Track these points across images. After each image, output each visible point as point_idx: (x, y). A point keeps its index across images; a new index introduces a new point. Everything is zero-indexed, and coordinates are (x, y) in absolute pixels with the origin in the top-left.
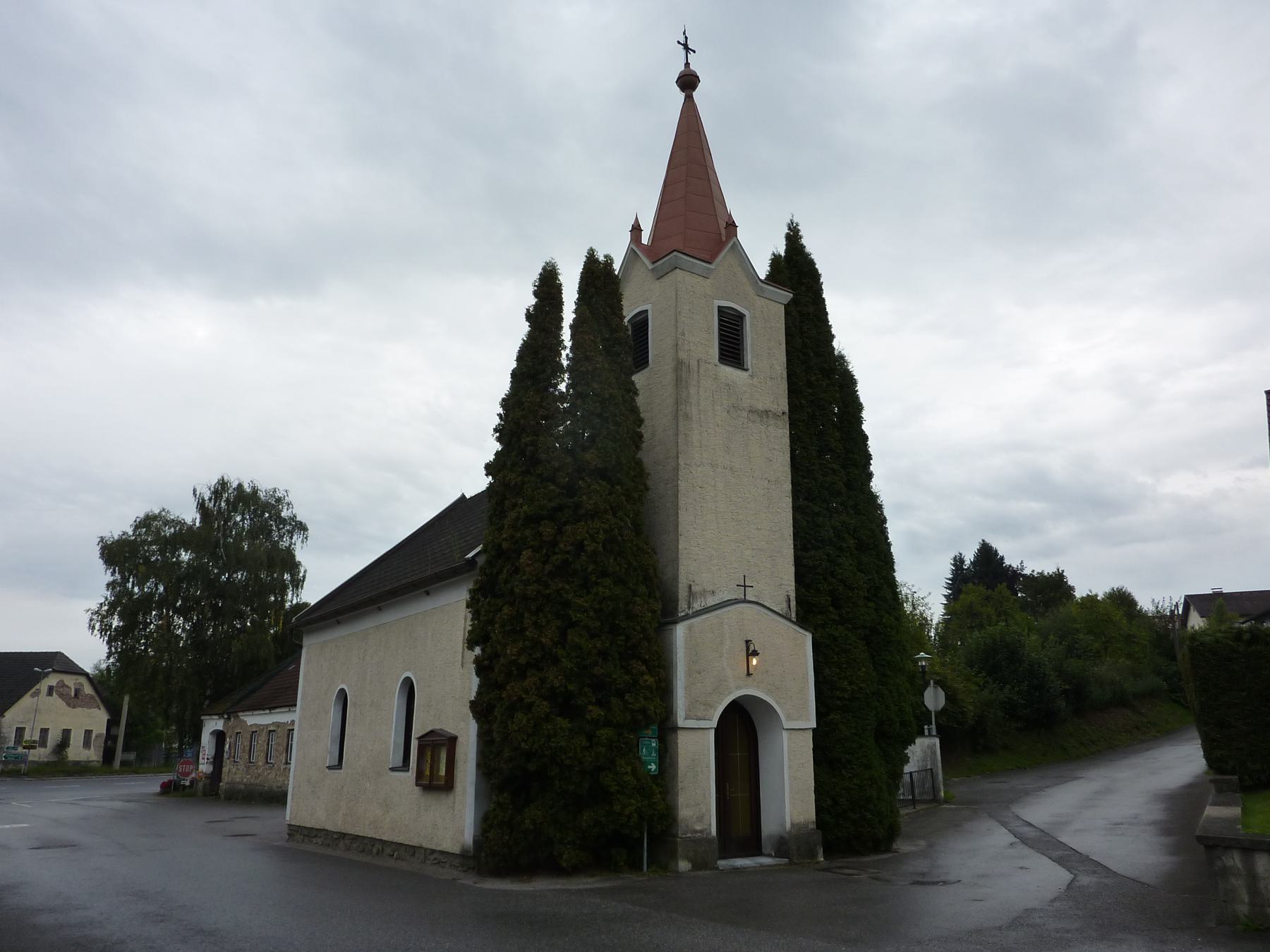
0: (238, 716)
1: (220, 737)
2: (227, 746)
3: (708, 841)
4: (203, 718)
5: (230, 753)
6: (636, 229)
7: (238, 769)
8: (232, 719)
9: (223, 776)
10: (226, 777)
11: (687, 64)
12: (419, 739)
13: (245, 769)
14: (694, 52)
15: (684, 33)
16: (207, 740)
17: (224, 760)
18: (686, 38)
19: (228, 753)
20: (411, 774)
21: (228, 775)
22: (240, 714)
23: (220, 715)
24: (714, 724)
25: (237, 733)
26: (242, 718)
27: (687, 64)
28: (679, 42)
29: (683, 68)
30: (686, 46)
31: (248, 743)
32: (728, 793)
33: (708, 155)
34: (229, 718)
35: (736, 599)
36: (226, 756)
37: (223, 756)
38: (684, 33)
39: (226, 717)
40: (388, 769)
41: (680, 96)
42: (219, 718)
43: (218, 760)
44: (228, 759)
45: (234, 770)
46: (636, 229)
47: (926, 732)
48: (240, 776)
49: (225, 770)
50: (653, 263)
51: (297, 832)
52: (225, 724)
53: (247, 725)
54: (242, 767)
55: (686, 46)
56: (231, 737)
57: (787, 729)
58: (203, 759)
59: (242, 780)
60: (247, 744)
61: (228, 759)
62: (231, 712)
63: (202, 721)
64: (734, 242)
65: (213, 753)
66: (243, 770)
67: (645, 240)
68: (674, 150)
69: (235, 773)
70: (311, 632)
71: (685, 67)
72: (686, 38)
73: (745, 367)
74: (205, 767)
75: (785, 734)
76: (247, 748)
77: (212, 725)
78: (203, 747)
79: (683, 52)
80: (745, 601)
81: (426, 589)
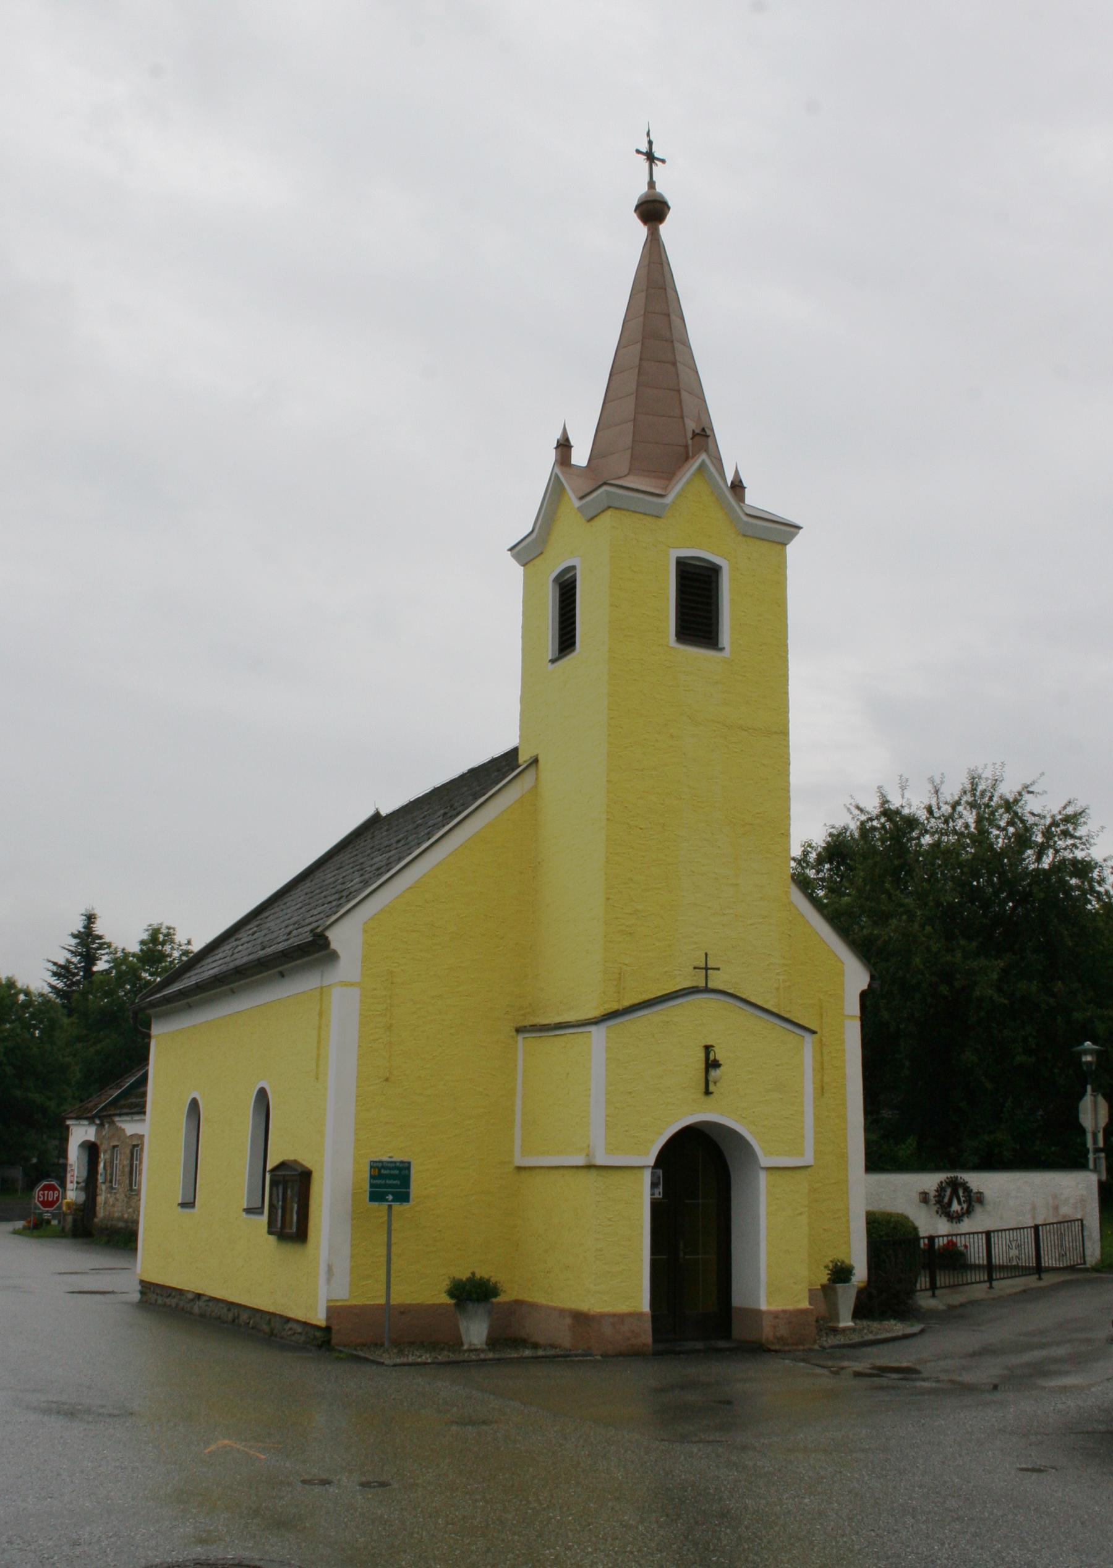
0: (112, 1123)
1: (91, 1150)
2: (102, 1165)
3: (639, 1315)
4: (68, 1122)
5: (106, 1174)
6: (564, 446)
7: (117, 1200)
8: (107, 1126)
9: (98, 1208)
10: (102, 1211)
11: (651, 184)
12: (273, 1170)
13: (125, 1199)
14: (663, 161)
15: (648, 134)
16: (74, 1154)
17: (99, 1185)
18: (650, 143)
19: (104, 1175)
20: (265, 1218)
21: (105, 1209)
22: (117, 1119)
23: (91, 1120)
24: (651, 1160)
25: (115, 1147)
26: (119, 1125)
27: (651, 184)
28: (638, 152)
29: (644, 189)
30: (650, 157)
31: (128, 1162)
32: (681, 1255)
33: (679, 321)
34: (102, 1125)
35: (693, 987)
36: (100, 1179)
37: (97, 1180)
38: (648, 134)
39: (98, 1122)
40: (241, 1210)
41: (641, 231)
42: (89, 1124)
43: (90, 1185)
44: (103, 1183)
45: (111, 1201)
46: (564, 446)
47: (1091, 1165)
48: (120, 1209)
49: (101, 1199)
50: (582, 498)
51: (147, 1287)
52: (97, 1132)
53: (125, 1134)
54: (121, 1196)
55: (650, 157)
56: (105, 1152)
57: (768, 1169)
58: (72, 1182)
59: (123, 1214)
60: (126, 1162)
61: (104, 1183)
62: (104, 1116)
63: (68, 1127)
64: (703, 462)
65: (84, 1174)
66: (123, 1201)
67: (580, 456)
68: (627, 319)
69: (113, 1205)
70: (165, 1015)
71: (649, 189)
72: (650, 143)
73: (720, 646)
74: (73, 1194)
75: (763, 1178)
76: (127, 1169)
77: (80, 1133)
78: (71, 1165)
79: (646, 165)
80: (707, 990)
81: (280, 969)
